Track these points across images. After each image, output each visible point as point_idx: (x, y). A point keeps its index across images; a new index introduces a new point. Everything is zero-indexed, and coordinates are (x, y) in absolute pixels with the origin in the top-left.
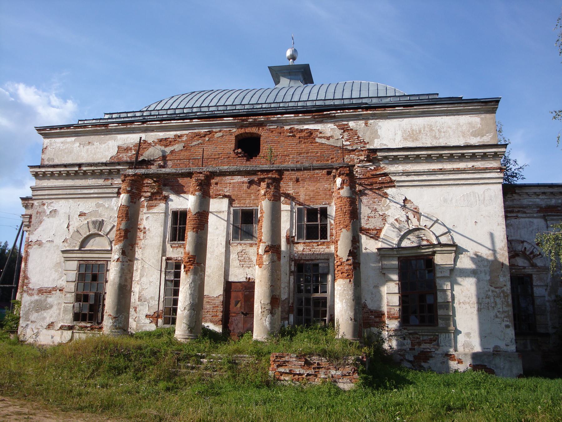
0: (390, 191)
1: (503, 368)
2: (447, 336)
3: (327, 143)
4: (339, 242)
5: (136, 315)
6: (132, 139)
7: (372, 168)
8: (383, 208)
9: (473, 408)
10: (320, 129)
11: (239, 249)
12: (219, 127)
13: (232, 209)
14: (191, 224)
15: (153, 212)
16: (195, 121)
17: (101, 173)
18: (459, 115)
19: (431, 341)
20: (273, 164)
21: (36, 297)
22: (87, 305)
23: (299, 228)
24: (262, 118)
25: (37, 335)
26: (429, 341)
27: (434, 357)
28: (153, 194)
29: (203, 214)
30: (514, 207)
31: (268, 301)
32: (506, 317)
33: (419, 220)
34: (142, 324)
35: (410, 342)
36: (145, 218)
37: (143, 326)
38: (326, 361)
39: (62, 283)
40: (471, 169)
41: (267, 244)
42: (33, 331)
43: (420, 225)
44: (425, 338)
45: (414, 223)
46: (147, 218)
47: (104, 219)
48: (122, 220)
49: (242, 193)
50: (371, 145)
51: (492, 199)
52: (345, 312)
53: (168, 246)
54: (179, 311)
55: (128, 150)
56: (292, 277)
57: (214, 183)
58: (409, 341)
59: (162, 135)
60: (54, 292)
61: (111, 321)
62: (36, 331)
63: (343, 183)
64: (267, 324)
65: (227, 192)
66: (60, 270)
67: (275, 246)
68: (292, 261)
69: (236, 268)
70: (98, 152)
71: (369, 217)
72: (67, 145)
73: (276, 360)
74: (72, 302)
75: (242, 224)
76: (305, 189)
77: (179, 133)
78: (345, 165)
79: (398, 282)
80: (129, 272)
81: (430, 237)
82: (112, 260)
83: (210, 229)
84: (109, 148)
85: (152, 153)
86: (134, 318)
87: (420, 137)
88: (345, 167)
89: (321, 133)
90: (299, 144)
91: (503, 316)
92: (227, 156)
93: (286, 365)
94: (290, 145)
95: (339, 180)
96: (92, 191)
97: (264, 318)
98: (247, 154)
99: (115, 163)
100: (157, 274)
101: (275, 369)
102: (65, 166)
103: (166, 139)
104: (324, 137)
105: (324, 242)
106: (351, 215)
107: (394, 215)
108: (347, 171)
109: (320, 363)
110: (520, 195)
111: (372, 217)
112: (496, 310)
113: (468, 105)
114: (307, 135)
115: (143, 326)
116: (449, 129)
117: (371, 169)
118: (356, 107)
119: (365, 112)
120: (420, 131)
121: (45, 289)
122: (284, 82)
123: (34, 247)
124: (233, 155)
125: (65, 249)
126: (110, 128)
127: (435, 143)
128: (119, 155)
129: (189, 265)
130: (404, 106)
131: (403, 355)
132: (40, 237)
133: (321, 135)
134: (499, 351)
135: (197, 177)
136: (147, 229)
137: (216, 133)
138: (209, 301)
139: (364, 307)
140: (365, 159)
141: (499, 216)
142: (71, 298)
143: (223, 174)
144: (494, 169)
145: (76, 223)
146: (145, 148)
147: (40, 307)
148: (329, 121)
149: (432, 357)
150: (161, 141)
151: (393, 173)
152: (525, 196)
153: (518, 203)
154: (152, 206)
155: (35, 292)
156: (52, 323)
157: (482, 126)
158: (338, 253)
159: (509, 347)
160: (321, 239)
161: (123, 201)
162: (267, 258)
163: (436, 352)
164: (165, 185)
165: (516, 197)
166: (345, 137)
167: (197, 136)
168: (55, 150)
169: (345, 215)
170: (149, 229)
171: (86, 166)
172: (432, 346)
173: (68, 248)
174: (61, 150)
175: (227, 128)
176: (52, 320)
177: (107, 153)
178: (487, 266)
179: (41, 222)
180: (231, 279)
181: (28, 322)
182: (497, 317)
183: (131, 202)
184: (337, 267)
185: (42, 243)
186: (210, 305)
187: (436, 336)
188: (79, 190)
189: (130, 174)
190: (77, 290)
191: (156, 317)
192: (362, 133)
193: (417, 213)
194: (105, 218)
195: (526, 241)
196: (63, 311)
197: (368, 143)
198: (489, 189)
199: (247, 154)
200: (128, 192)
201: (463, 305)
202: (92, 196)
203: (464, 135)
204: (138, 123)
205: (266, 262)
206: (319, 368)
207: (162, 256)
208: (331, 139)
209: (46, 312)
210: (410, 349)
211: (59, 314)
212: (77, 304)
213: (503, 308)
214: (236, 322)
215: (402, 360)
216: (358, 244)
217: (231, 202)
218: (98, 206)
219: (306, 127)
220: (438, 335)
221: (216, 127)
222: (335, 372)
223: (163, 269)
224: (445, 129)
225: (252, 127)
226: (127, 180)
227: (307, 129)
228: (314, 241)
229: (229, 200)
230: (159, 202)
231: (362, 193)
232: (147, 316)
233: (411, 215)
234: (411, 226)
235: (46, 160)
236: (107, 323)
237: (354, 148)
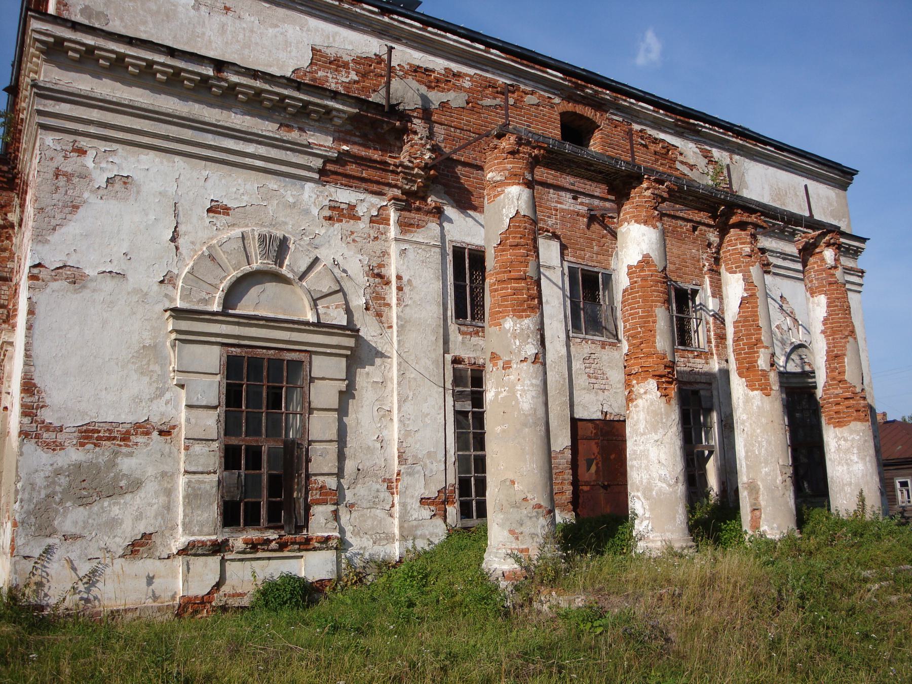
9: (80, 637)
10: (680, 146)
12: (531, 83)
13: (566, 264)
18: (818, 181)
21: (74, 455)
24: (607, 95)
25: (91, 579)
34: (415, 523)
37: (416, 527)
42: (74, 569)
53: (453, 328)
55: (339, 66)
60: (141, 439)
62: (84, 568)
69: (584, 392)
70: (257, 44)
74: (211, 469)
77: (455, 67)
86: (388, 507)
89: (681, 154)
96: (251, 148)
102: (172, 52)
103: (426, 70)
115: (416, 527)
119: (734, 140)
121: (107, 426)
123: (55, 285)
137: (527, 94)
148: (690, 137)
151: (772, 251)
154: (411, 225)
155: (69, 438)
156: (146, 536)
167: (489, 86)
170: (409, 281)
171: (238, 73)
175: (545, 91)
176: (142, 527)
177: (282, 55)
179: (76, 207)
180: (577, 416)
181: (50, 541)
185: (84, 276)
188: (210, 136)
191: (443, 503)
196: (187, 497)
202: (248, 161)
209: (118, 503)
219: (662, 136)
221: (527, 82)
225: (586, 105)
227: (663, 141)
230: (426, 218)
232: (424, 501)
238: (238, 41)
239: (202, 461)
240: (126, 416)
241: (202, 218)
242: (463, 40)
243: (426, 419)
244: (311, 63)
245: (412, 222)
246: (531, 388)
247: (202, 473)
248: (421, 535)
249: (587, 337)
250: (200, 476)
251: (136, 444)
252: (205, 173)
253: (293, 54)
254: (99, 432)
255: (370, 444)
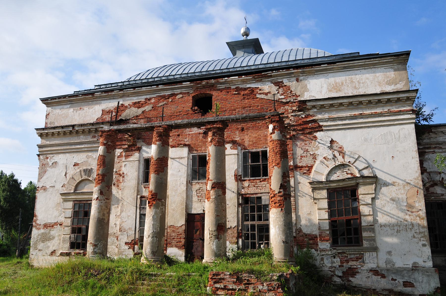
0: (318, 134)
1: (422, 282)
2: (371, 254)
3: (265, 98)
4: (272, 178)
5: (118, 243)
6: (112, 104)
7: (304, 116)
8: (313, 149)
11: (198, 187)
14: (153, 168)
15: (130, 160)
16: (161, 87)
17: (90, 131)
19: (357, 259)
20: (218, 116)
21: (42, 231)
22: (80, 235)
23: (245, 168)
26: (355, 259)
27: (360, 273)
28: (129, 146)
29: (163, 159)
30: (432, 144)
31: (214, 229)
32: (423, 237)
33: (343, 157)
34: (123, 250)
35: (339, 260)
36: (123, 166)
37: (123, 252)
38: (255, 277)
39: (61, 219)
40: (386, 112)
41: (213, 181)
43: (344, 161)
44: (352, 256)
45: (340, 161)
46: (125, 165)
47: (92, 167)
48: (100, 167)
49: (199, 142)
50: (302, 97)
51: (407, 136)
52: (278, 236)
54: (145, 239)
56: (240, 209)
57: (177, 135)
58: (339, 260)
59: (135, 99)
60: (55, 226)
61: (92, 248)
63: (274, 129)
64: (214, 247)
65: (187, 141)
66: (60, 208)
67: (220, 183)
68: (240, 195)
71: (302, 157)
72: (64, 111)
73: (213, 277)
74: (69, 234)
75: (199, 167)
76: (249, 136)
78: (275, 114)
79: (327, 210)
80: (106, 209)
81: (354, 171)
82: (93, 199)
83: (170, 172)
84: (95, 112)
85: (128, 114)
87: (343, 88)
88: (276, 115)
89: (260, 90)
90: (243, 100)
91: (420, 236)
92: (186, 113)
93: (222, 282)
94: (236, 101)
95: (271, 127)
97: (211, 243)
98: (202, 111)
99: (100, 123)
100: (133, 210)
101: (212, 285)
102: (62, 127)
104: (263, 93)
105: (265, 179)
106: (281, 155)
107: (323, 154)
108: (277, 119)
109: (250, 280)
110: (436, 134)
111: (304, 157)
112: (413, 232)
113: (383, 59)
114: (249, 92)
115: (123, 252)
116: (367, 80)
117: (302, 117)
118: (288, 68)
120: (342, 84)
122: (240, 53)
123: (41, 191)
124: (191, 112)
125: (63, 192)
126: (96, 95)
127: (355, 93)
128: (103, 117)
129: (152, 201)
130: (328, 64)
131: (334, 272)
132: (45, 184)
133: (261, 92)
134: (418, 267)
135: (157, 130)
136: (125, 174)
138: (174, 230)
139: (299, 232)
140: (297, 109)
141: (413, 150)
142: (68, 230)
143: (178, 126)
144: (407, 111)
145: (72, 171)
146: (123, 110)
147: (45, 238)
148: (266, 80)
149: (358, 272)
150: (135, 104)
152: (441, 134)
153: (435, 140)
154: (129, 156)
155: (42, 227)
156: (55, 250)
157: (396, 76)
158: (271, 187)
159: (426, 263)
160: (263, 176)
161: (101, 152)
162: (214, 193)
163: (362, 268)
164: (138, 139)
165: (432, 135)
166: (280, 92)
168: (56, 115)
169: (276, 155)
170: (126, 174)
172: (358, 263)
173: (65, 192)
174: (60, 116)
176: (54, 249)
177: (94, 116)
178: (404, 193)
179: (46, 172)
182: (414, 237)
183: (107, 152)
184: (271, 199)
186: (175, 233)
187: (361, 255)
189: (106, 130)
190: (73, 224)
191: (133, 244)
192: (294, 88)
193: (342, 153)
194: (94, 167)
195: (443, 173)
196: (63, 241)
197: (299, 96)
198: (403, 128)
199: (202, 111)
200: (104, 144)
201: (384, 228)
203: (380, 84)
204: (117, 91)
205: (212, 196)
206: (249, 284)
207: (137, 195)
208: (269, 94)
209: (50, 242)
210: (339, 266)
211: (60, 243)
212: (73, 236)
213: (419, 229)
214: (196, 246)
215: (332, 276)
216: (288, 179)
217: (191, 149)
218: (88, 157)
220: (363, 254)
222: (262, 287)
223: (138, 206)
224: (363, 80)
226: (104, 135)
228: (257, 178)
229: (189, 148)
231: (294, 138)
232: (126, 243)
233: (337, 154)
234: (337, 162)
235: (48, 124)
236: (90, 248)
237: (288, 101)
238: (83, 116)
239: (67, 232)
240: (53, 221)
241: (72, 168)
242: (148, 87)
243: (129, 217)
244: (102, 115)
245: (129, 154)
246: (94, 208)
247: (67, 235)
248: (125, 254)
249: (199, 181)
250: (66, 236)
251: (55, 228)
252: (73, 156)
253: (97, 114)
254: (47, 225)
255: (113, 226)
